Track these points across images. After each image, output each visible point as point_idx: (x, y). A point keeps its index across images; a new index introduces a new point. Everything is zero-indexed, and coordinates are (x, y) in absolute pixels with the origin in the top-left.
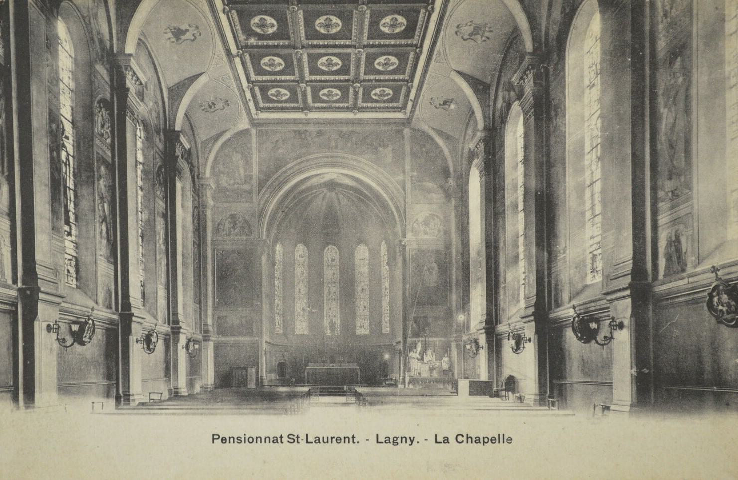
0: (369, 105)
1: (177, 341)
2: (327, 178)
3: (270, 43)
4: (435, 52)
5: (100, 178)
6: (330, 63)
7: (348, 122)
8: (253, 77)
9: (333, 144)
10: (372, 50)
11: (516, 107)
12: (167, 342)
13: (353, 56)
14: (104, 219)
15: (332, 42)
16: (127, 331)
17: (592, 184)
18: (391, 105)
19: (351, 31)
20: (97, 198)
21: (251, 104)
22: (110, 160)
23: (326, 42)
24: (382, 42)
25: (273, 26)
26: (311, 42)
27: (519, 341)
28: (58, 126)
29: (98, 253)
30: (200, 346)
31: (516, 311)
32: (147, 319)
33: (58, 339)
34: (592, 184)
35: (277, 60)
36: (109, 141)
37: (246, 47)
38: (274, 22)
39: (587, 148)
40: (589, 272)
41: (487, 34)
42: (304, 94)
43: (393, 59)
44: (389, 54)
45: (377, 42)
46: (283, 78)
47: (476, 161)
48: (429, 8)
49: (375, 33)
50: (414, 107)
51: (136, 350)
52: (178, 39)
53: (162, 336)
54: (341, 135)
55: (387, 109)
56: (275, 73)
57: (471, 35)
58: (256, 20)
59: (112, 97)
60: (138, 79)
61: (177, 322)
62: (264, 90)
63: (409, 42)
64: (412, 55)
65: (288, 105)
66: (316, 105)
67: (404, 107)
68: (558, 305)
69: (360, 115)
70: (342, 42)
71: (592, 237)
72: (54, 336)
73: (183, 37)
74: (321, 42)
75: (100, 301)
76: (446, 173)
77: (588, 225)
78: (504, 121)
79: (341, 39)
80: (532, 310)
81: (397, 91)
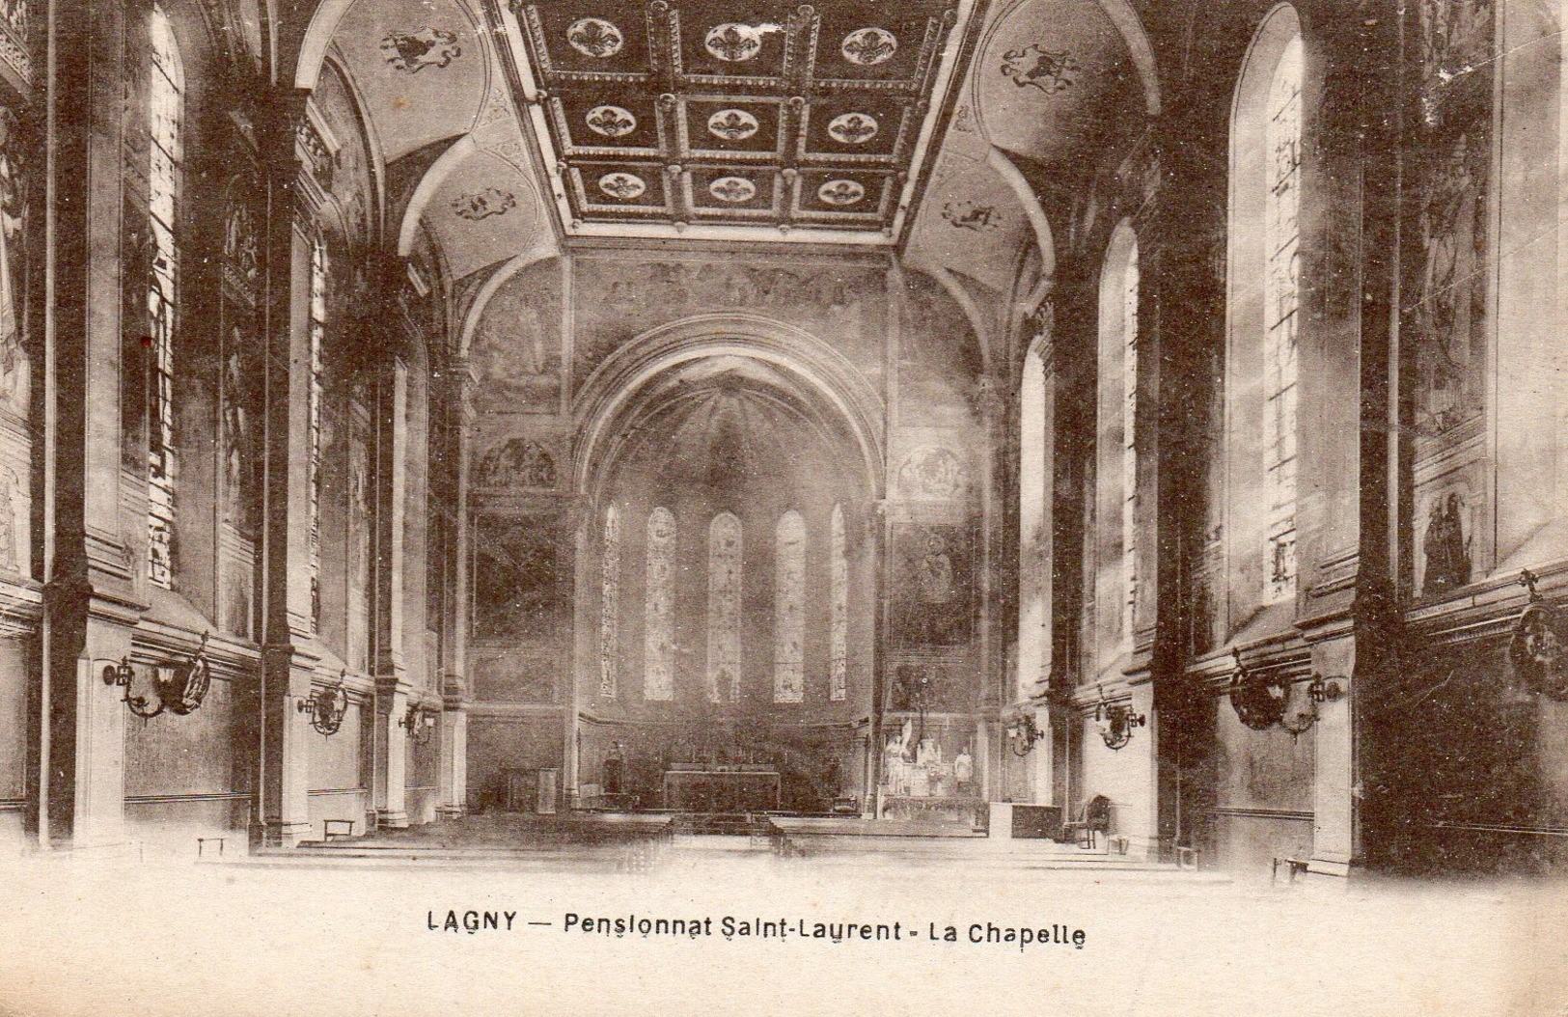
1: (387, 707)
2: (721, 366)
6: (734, 125)
11: (1124, 233)
12: (365, 710)
21: (563, 205)
29: (221, 515)
31: (1115, 658)
33: (127, 699)
46: (633, 151)
50: (908, 223)
51: (298, 728)
57: (1031, 75)
60: (320, 143)
62: (593, 171)
63: (883, 158)
67: (889, 221)
72: (119, 692)
75: (223, 619)
80: (1146, 658)
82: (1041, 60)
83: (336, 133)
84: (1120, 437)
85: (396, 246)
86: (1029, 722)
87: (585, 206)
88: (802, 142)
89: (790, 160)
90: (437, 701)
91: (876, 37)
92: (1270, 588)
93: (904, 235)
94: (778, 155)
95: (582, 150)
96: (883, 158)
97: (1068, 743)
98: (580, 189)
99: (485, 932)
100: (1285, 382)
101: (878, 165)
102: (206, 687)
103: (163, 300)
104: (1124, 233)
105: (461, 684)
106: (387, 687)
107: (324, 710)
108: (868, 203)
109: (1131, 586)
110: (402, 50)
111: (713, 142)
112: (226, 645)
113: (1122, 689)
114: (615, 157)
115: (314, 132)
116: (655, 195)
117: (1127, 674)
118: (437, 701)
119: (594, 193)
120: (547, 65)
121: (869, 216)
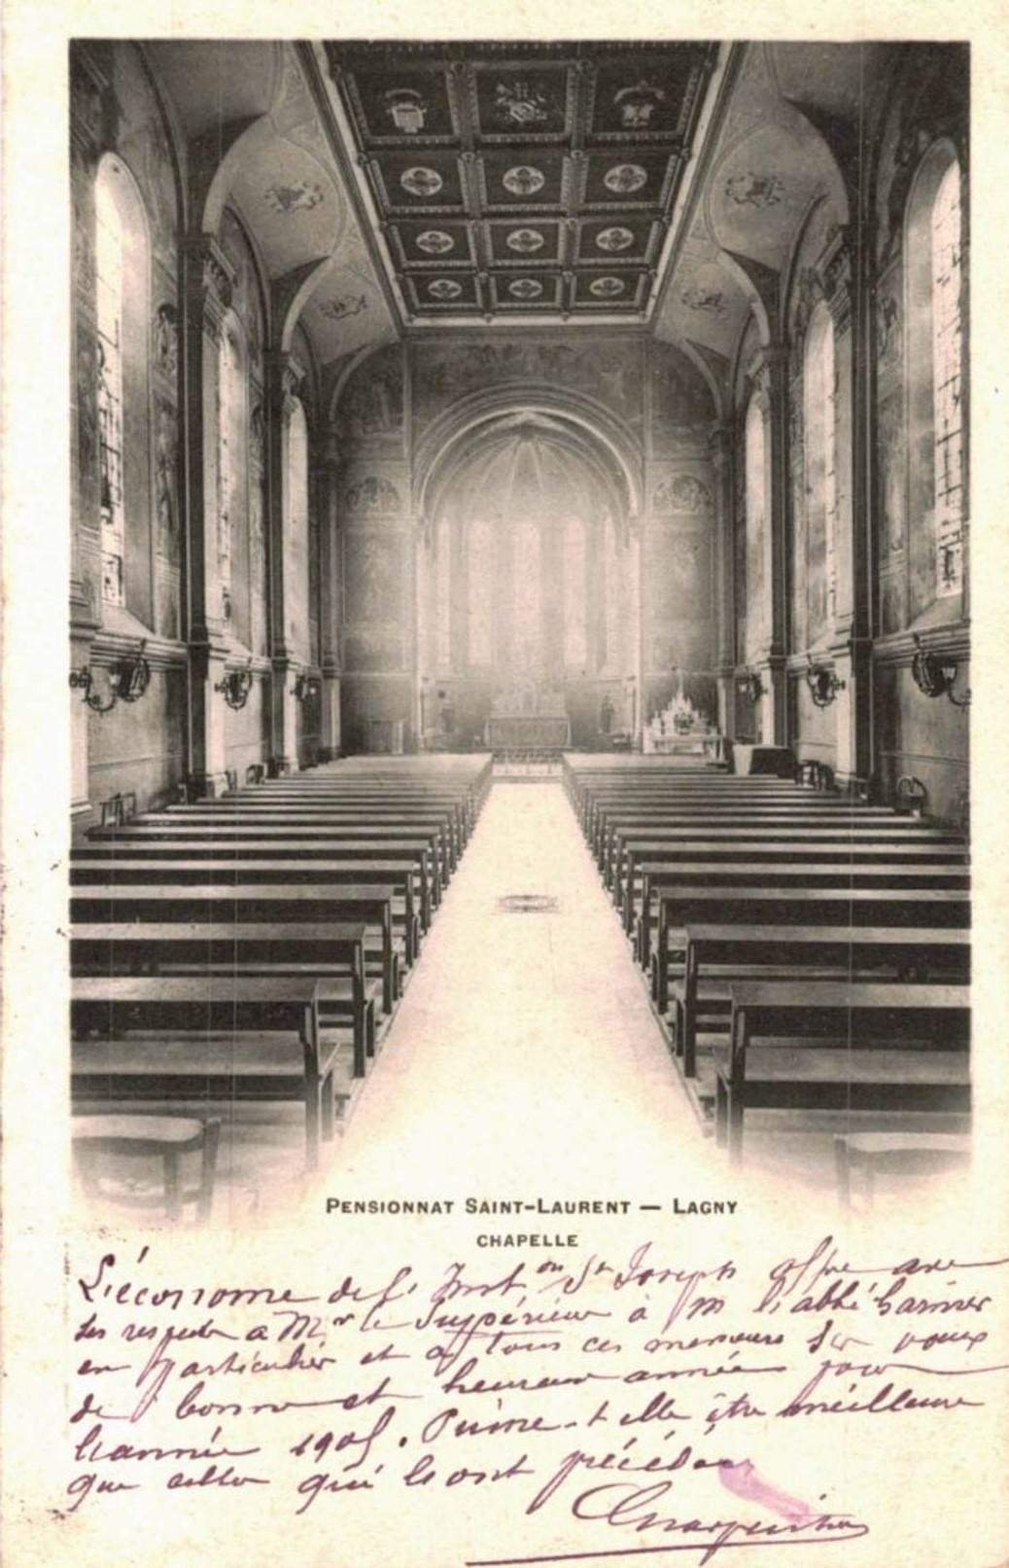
0: (586, 304)
1: (282, 682)
2: (519, 420)
3: (432, 209)
4: (693, 223)
5: (158, 432)
6: (527, 242)
7: (554, 331)
8: (405, 263)
9: (530, 368)
10: (590, 220)
11: (822, 308)
12: (266, 684)
13: (562, 229)
14: (166, 496)
15: (528, 208)
16: (202, 673)
17: (946, 439)
18: (621, 304)
19: (558, 189)
20: (154, 463)
21: (401, 305)
22: (174, 402)
23: (520, 208)
24: (608, 206)
25: (435, 184)
26: (494, 208)
27: (825, 684)
28: (93, 355)
29: (156, 549)
30: (318, 688)
31: (825, 635)
32: (235, 646)
33: (87, 699)
34: (946, 439)
35: (443, 237)
36: (175, 372)
37: (394, 215)
38: (438, 177)
39: (939, 381)
40: (940, 577)
41: (776, 193)
42: (485, 288)
43: (626, 233)
44: (621, 225)
45: (600, 206)
46: (451, 263)
47: (757, 395)
48: (684, 152)
49: (596, 191)
50: (656, 309)
51: (216, 705)
52: (287, 206)
53: (257, 677)
54: (542, 351)
55: (614, 311)
56: (443, 257)
57: (749, 194)
58: (410, 174)
59: (180, 301)
60: (222, 273)
61: (282, 652)
62: (422, 280)
63: (638, 260)
64: (642, 278)
65: (459, 305)
66: (503, 305)
67: (644, 307)
68: (889, 630)
69: (575, 320)
70: (545, 207)
71: (945, 523)
72: (82, 692)
73: (295, 203)
74: (511, 208)
75: (158, 626)
76: (710, 413)
77: (940, 502)
78: (803, 333)
79: (544, 202)
80: (846, 637)
81: (631, 280)
82: (756, 184)
84: (822, 467)
85: (279, 345)
86: (756, 680)
87: (418, 305)
88: (577, 249)
90: (318, 673)
92: (942, 584)
93: (655, 317)
95: (413, 264)
96: (638, 260)
98: (413, 293)
100: (952, 429)
101: (632, 265)
102: (147, 681)
103: (109, 396)
104: (822, 308)
105: (334, 658)
106: (280, 665)
107: (234, 687)
108: (628, 294)
109: (831, 579)
110: (281, 199)
112: (161, 645)
113: (826, 658)
114: (439, 268)
115: (216, 264)
116: (468, 294)
117: (832, 649)
118: (318, 673)
119: (425, 296)
120: (387, 203)
121: (627, 303)
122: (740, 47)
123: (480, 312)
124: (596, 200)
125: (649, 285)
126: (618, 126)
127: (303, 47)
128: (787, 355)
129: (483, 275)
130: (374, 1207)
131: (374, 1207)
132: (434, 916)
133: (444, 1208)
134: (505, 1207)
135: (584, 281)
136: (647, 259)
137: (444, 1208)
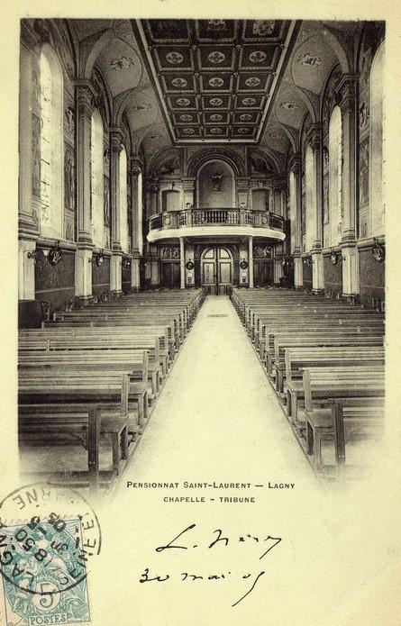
63: (262, 90)
67: (255, 137)
81: (255, 115)
83: (217, 266)
89: (241, 42)
91: (259, 54)
94: (232, 68)
96: (262, 90)
97: (34, 593)
99: (285, 489)
111: (210, 88)
118: (108, 252)
122: (299, 22)
123: (200, 138)
124: (243, 89)
125: (261, 117)
126: (240, 120)
127: (133, 21)
128: (321, 130)
129: (199, 96)
130: (146, 485)
131: (146, 485)
132: (130, 449)
133: (175, 485)
134: (200, 485)
135: (236, 129)
136: (265, 90)
137: (175, 485)
